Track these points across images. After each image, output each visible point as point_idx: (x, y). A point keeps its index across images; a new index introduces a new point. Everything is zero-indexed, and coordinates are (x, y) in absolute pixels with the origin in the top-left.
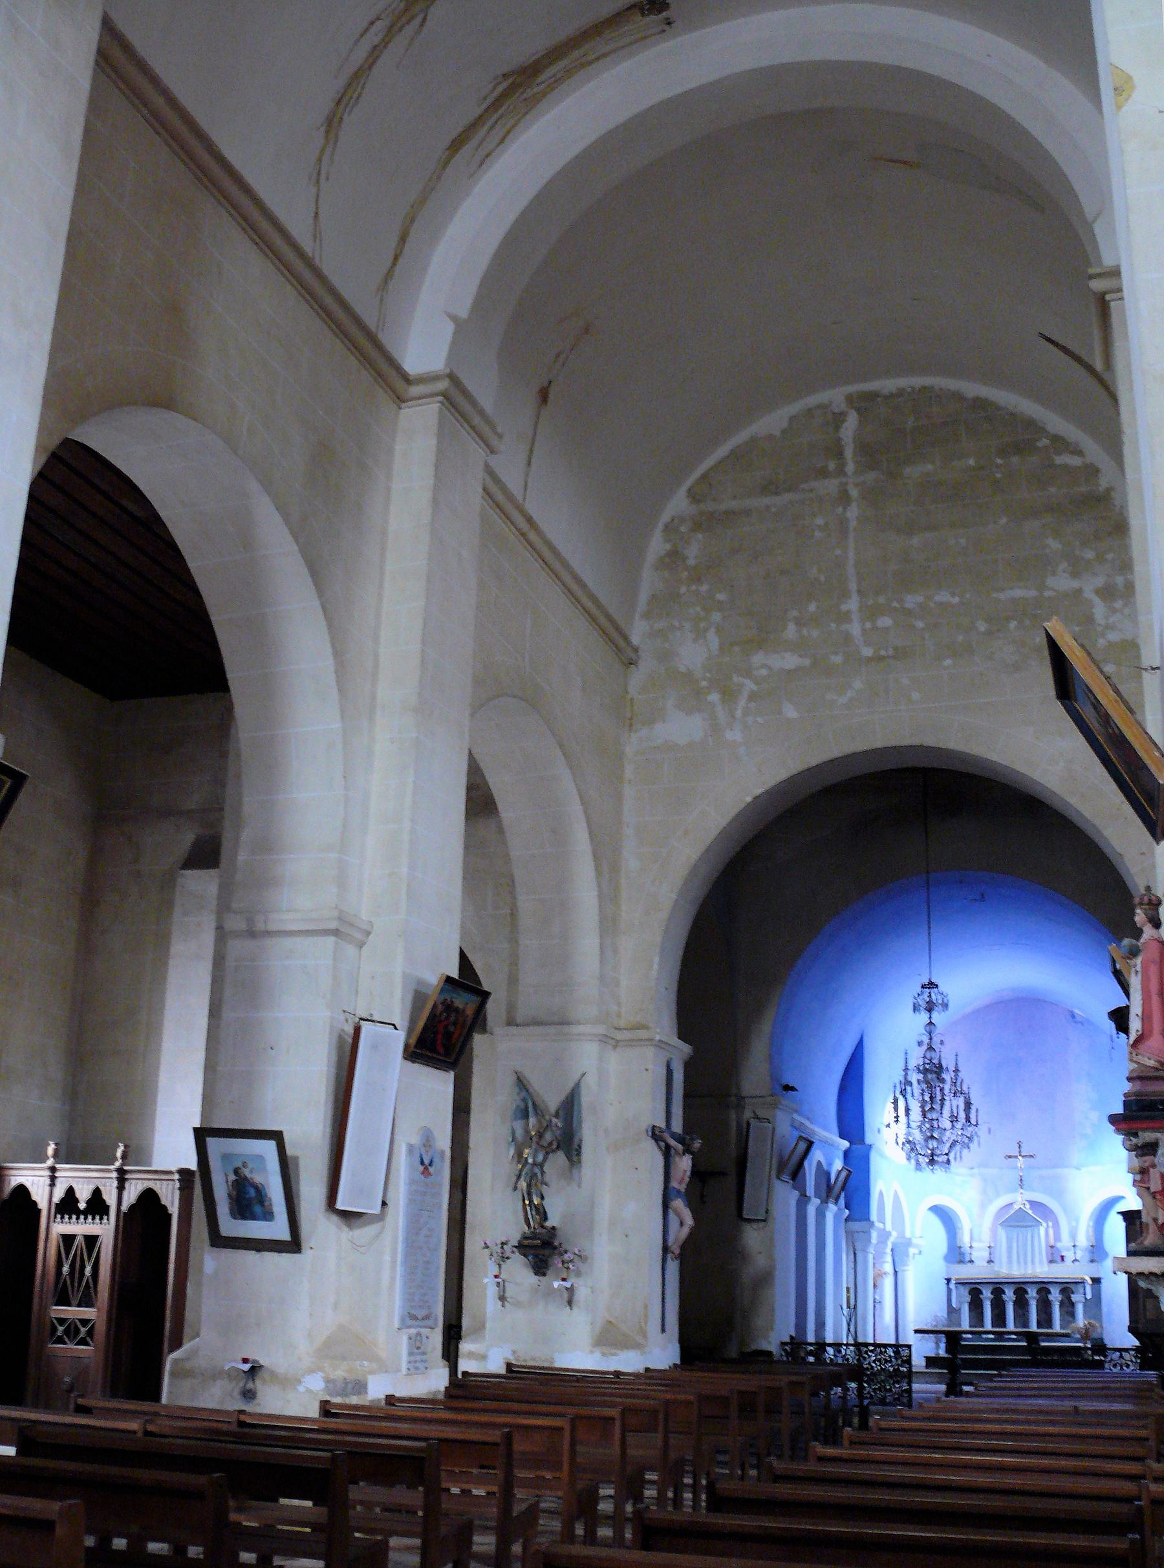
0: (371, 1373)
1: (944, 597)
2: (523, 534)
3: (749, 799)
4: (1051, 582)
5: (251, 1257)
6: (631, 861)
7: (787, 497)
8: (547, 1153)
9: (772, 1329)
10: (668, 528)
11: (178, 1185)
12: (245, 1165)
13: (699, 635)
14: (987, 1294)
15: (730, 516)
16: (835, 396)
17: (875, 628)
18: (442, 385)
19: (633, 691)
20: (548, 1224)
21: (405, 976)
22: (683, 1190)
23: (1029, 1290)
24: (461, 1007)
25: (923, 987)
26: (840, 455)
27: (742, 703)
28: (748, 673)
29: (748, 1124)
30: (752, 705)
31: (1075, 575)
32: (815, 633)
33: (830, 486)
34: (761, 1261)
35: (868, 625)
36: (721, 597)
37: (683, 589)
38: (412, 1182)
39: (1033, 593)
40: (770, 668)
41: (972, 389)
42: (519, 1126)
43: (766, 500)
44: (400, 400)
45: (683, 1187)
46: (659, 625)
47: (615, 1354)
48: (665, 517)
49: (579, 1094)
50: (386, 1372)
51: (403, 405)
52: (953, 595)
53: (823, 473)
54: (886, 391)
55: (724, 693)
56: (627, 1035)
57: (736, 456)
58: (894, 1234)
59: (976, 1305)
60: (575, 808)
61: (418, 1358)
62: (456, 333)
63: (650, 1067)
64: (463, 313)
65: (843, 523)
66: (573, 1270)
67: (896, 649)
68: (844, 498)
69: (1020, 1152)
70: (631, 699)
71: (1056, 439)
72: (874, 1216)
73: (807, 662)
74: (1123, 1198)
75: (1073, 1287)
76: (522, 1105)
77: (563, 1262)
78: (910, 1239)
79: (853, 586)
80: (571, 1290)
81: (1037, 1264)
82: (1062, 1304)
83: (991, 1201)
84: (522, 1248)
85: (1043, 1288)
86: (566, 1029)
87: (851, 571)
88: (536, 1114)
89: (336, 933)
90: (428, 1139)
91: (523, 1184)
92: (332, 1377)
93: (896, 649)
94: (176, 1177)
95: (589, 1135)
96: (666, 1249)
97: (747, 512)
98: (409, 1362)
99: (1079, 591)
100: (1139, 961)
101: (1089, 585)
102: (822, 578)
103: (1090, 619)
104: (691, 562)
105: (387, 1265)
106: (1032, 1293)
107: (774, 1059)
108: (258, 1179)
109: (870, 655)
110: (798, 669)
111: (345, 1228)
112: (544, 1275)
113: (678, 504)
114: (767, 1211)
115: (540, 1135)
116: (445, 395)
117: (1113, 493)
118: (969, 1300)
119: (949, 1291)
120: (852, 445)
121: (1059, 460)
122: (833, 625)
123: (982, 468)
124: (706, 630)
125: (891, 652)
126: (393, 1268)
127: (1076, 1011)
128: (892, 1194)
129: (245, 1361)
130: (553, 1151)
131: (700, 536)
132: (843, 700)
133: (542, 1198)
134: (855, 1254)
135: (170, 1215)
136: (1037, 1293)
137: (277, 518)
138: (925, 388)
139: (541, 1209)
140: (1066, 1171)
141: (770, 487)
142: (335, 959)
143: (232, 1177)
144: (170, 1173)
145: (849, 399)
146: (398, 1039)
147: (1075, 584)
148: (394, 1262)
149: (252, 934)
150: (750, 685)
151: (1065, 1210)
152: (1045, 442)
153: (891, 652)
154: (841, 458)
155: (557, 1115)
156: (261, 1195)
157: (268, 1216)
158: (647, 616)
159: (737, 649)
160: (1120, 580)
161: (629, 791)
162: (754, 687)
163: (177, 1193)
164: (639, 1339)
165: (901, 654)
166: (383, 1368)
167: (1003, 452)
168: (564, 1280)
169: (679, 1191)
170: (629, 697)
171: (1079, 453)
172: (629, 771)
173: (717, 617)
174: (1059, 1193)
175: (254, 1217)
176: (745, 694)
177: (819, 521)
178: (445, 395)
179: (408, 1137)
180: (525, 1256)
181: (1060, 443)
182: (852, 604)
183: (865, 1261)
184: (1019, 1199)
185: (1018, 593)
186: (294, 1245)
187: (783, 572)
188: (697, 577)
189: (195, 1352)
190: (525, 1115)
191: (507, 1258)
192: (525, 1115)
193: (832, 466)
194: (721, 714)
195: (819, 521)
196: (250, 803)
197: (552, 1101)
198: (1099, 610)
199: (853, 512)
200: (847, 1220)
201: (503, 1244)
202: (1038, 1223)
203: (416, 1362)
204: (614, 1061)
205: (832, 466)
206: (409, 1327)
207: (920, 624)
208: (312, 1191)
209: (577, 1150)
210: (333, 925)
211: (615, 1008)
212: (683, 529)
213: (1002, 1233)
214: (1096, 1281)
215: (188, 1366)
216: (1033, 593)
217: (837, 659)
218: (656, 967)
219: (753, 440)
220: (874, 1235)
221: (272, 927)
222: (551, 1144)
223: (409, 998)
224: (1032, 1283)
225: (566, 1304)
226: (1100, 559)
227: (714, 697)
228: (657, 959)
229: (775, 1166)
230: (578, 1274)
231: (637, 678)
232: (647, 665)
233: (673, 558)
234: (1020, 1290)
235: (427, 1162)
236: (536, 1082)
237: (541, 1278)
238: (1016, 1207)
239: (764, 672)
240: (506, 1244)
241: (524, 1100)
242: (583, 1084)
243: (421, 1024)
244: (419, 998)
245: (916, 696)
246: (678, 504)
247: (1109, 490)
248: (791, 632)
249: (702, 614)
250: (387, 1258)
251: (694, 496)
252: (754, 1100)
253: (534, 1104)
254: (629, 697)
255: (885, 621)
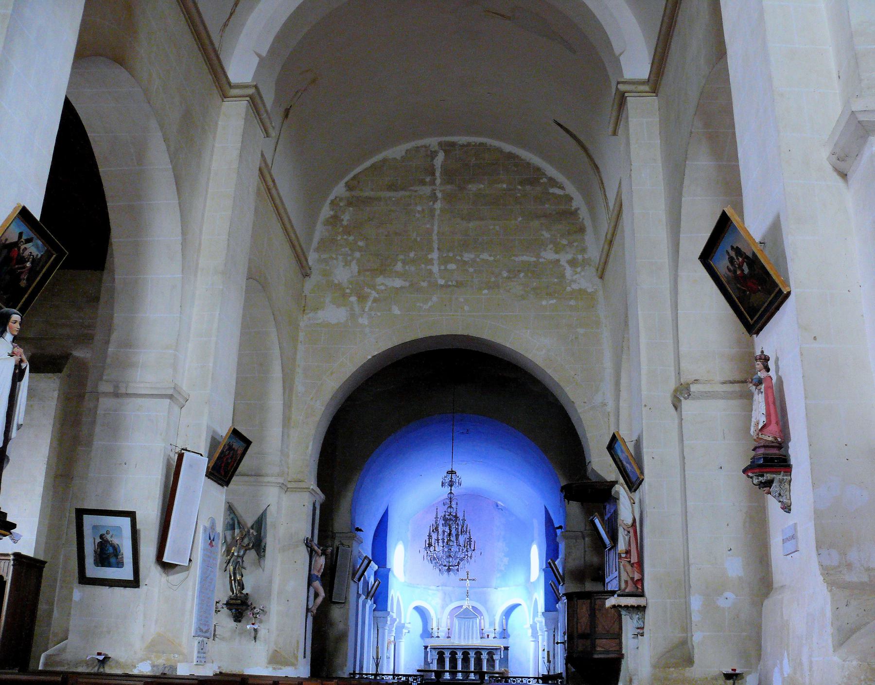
0: (179, 662)
1: (485, 256)
2: (269, 189)
3: (370, 357)
4: (543, 254)
5: (105, 590)
6: (299, 387)
7: (401, 193)
8: (246, 550)
9: (346, 666)
10: (332, 202)
11: (12, 562)
12: (108, 532)
13: (347, 264)
14: (447, 655)
15: (369, 201)
16: (432, 142)
17: (446, 269)
18: (251, 91)
19: (306, 292)
20: (244, 592)
21: (208, 427)
22: (319, 576)
23: (470, 653)
24: (236, 449)
25: (447, 473)
26: (433, 174)
27: (369, 303)
28: (373, 287)
29: (338, 548)
30: (375, 305)
31: (557, 252)
32: (413, 269)
33: (427, 190)
34: (341, 626)
35: (443, 267)
36: (361, 244)
37: (339, 238)
38: (204, 550)
39: (533, 259)
40: (386, 286)
41: (508, 148)
42: (229, 533)
43: (392, 194)
44: (224, 96)
45: (319, 575)
46: (324, 256)
47: (281, 669)
48: (332, 197)
49: (266, 516)
50: (187, 662)
51: (225, 100)
52: (490, 256)
53: (422, 183)
54: (460, 143)
55: (359, 297)
56: (294, 485)
57: (374, 167)
58: (398, 620)
59: (441, 661)
60: (276, 351)
61: (202, 655)
62: (259, 63)
63: (306, 504)
64: (264, 54)
65: (432, 211)
66: (259, 618)
67: (457, 282)
68: (434, 197)
69: (468, 577)
70: (306, 296)
71: (551, 179)
72: (389, 610)
73: (407, 284)
74: (520, 605)
75: (494, 651)
76: (231, 522)
77: (253, 614)
78: (404, 624)
79: (436, 246)
80: (256, 630)
81: (474, 639)
82: (488, 660)
83: (447, 605)
84: (228, 604)
85: (478, 652)
86: (261, 479)
87: (435, 237)
88: (240, 528)
89: (171, 397)
90: (213, 527)
91: (231, 568)
92: (156, 663)
93: (457, 282)
94: (12, 557)
95: (271, 541)
96: (308, 610)
97: (379, 199)
98: (198, 657)
99: (558, 261)
100: (763, 386)
101: (564, 258)
102: (419, 239)
103: (563, 276)
104: (345, 223)
105: (190, 598)
106: (472, 654)
107: (353, 511)
108: (115, 541)
109: (442, 284)
110: (402, 288)
111: (164, 575)
112: (240, 621)
113: (340, 190)
114: (346, 598)
115: (242, 539)
116: (251, 97)
117: (579, 212)
118: (437, 658)
119: (426, 654)
120: (440, 170)
121: (551, 190)
122: (423, 266)
123: (510, 190)
124: (351, 261)
125: (454, 283)
126: (193, 600)
127: (499, 503)
128: (397, 597)
129: (99, 654)
130: (250, 549)
131: (351, 209)
132: (426, 307)
133: (242, 576)
134: (378, 630)
135: (5, 582)
136: (475, 654)
137: (163, 147)
138: (482, 143)
139: (241, 582)
140: (489, 589)
141: (392, 187)
142: (169, 412)
143: (98, 540)
144: (8, 555)
145: (440, 144)
146: (204, 463)
147: (556, 257)
148: (193, 596)
149: (116, 395)
150: (374, 294)
151: (487, 611)
152: (544, 180)
153: (454, 283)
154: (434, 176)
155: (252, 527)
156: (116, 551)
157: (120, 564)
158: (317, 250)
159: (368, 273)
160: (580, 257)
161: (301, 348)
162: (377, 296)
163: (11, 568)
164: (293, 660)
165: (459, 285)
166: (186, 659)
167: (521, 183)
168: (253, 624)
169: (317, 576)
170: (304, 294)
171: (563, 188)
172: (301, 336)
173: (357, 255)
174: (485, 602)
175: (109, 565)
176: (372, 299)
177: (419, 208)
178: (251, 97)
179: (204, 523)
180: (231, 610)
181: (552, 182)
182: (435, 255)
183: (384, 633)
184: (466, 604)
185: (525, 258)
186: (135, 583)
187: (396, 234)
188: (347, 231)
189: (64, 650)
190: (233, 528)
191: (219, 611)
192: (233, 528)
193: (428, 179)
194: (357, 309)
195: (419, 208)
196: (119, 317)
197: (249, 520)
198: (568, 271)
199: (438, 205)
200: (374, 610)
201: (217, 603)
202: (475, 616)
203: (200, 657)
204: (286, 500)
205: (428, 179)
206: (199, 636)
207: (471, 270)
208: (148, 550)
209: (263, 549)
210: (170, 392)
211: (286, 469)
212: (341, 204)
213: (456, 621)
214: (506, 648)
215: (58, 659)
216: (533, 259)
217: (424, 284)
218: (310, 448)
219: (384, 161)
220: (389, 619)
221: (130, 391)
222: (248, 544)
223: (209, 440)
224: (473, 649)
225: (253, 639)
226: (570, 244)
227: (353, 299)
228: (311, 443)
229: (351, 573)
230: (261, 622)
231: (309, 284)
232: (315, 278)
233: (334, 221)
234: (466, 652)
235: (212, 539)
236: (240, 509)
237: (238, 624)
238: (464, 607)
239: (383, 288)
240: (218, 603)
241: (232, 519)
242: (268, 512)
243: (216, 455)
244: (214, 442)
245: (466, 308)
246: (340, 190)
247: (577, 210)
248: (399, 266)
249: (349, 252)
250: (190, 593)
251: (349, 187)
252: (341, 535)
253: (239, 523)
254: (304, 294)
255: (452, 266)
